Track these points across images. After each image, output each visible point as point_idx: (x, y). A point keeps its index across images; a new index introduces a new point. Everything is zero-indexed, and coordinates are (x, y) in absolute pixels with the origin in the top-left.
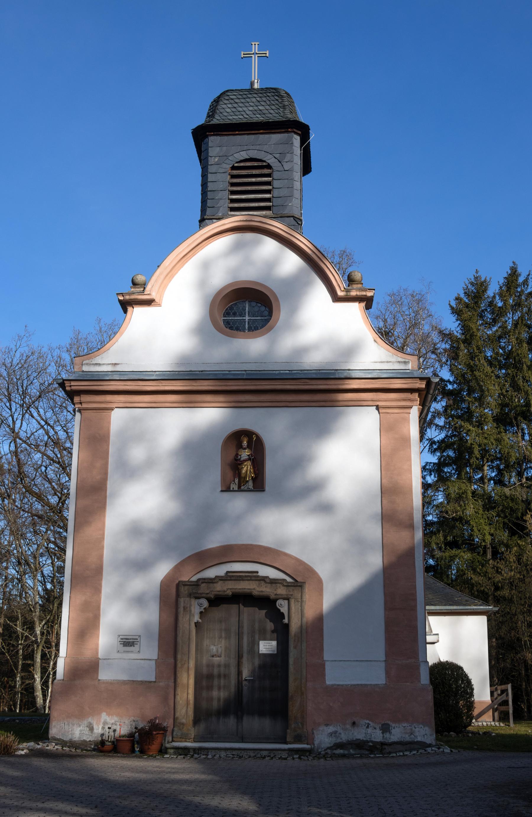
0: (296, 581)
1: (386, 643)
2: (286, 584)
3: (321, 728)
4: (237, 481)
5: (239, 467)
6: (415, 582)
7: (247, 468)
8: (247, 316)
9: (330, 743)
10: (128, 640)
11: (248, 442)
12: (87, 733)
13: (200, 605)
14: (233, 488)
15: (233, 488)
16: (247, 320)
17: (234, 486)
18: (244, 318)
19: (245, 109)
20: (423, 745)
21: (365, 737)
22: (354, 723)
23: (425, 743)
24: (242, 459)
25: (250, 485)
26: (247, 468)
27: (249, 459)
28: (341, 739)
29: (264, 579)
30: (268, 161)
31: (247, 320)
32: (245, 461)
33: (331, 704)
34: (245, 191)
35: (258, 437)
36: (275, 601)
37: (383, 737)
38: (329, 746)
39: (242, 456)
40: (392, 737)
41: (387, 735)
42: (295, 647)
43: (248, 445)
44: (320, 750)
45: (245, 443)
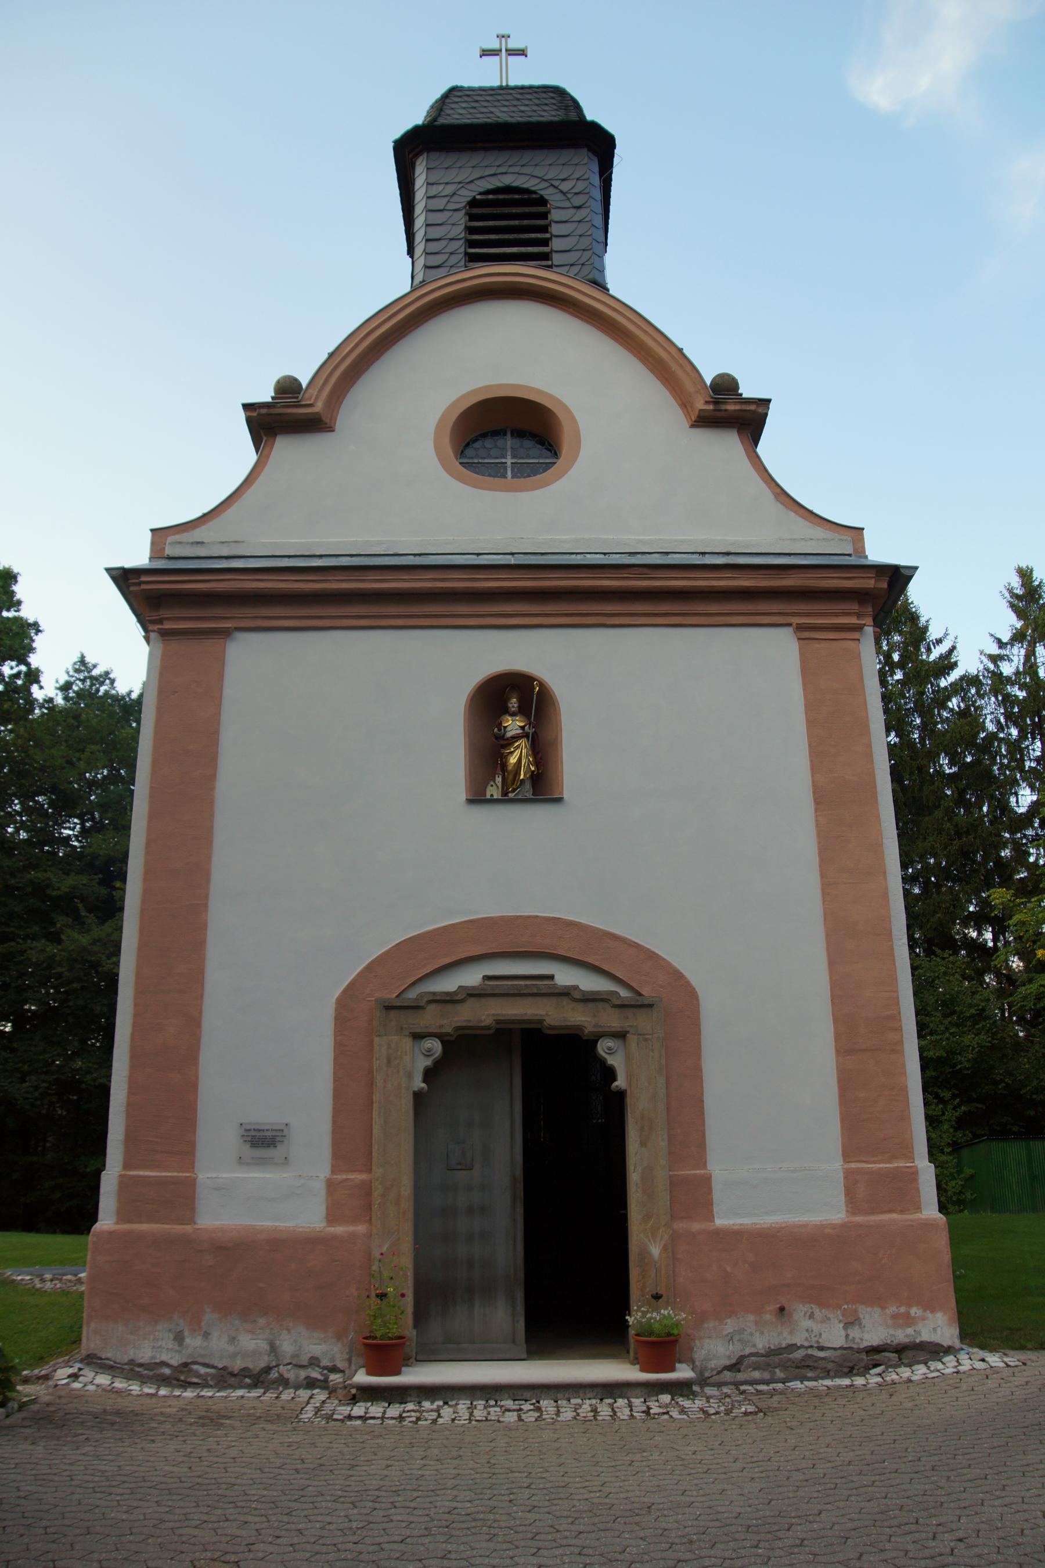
0: (640, 994)
1: (842, 1127)
2: (618, 1002)
3: (710, 1324)
4: (499, 780)
5: (503, 751)
6: (897, 991)
7: (518, 755)
8: (509, 457)
9: (729, 1357)
10: (262, 1134)
11: (520, 701)
12: (170, 1346)
13: (428, 1053)
14: (492, 795)
15: (492, 795)
16: (509, 464)
17: (494, 791)
18: (504, 461)
19: (492, 109)
20: (935, 1351)
21: (806, 1339)
22: (782, 1309)
23: (938, 1345)
24: (509, 734)
25: (527, 791)
26: (518, 755)
27: (526, 735)
28: (754, 1346)
29: (566, 993)
30: (542, 193)
31: (509, 464)
32: (516, 738)
33: (729, 1269)
34: (495, 206)
35: (542, 685)
36: (593, 1043)
37: (847, 1336)
38: (728, 1363)
39: (509, 729)
40: (866, 1336)
41: (855, 1333)
42: (643, 1144)
43: (519, 707)
44: (707, 1374)
45: (514, 703)
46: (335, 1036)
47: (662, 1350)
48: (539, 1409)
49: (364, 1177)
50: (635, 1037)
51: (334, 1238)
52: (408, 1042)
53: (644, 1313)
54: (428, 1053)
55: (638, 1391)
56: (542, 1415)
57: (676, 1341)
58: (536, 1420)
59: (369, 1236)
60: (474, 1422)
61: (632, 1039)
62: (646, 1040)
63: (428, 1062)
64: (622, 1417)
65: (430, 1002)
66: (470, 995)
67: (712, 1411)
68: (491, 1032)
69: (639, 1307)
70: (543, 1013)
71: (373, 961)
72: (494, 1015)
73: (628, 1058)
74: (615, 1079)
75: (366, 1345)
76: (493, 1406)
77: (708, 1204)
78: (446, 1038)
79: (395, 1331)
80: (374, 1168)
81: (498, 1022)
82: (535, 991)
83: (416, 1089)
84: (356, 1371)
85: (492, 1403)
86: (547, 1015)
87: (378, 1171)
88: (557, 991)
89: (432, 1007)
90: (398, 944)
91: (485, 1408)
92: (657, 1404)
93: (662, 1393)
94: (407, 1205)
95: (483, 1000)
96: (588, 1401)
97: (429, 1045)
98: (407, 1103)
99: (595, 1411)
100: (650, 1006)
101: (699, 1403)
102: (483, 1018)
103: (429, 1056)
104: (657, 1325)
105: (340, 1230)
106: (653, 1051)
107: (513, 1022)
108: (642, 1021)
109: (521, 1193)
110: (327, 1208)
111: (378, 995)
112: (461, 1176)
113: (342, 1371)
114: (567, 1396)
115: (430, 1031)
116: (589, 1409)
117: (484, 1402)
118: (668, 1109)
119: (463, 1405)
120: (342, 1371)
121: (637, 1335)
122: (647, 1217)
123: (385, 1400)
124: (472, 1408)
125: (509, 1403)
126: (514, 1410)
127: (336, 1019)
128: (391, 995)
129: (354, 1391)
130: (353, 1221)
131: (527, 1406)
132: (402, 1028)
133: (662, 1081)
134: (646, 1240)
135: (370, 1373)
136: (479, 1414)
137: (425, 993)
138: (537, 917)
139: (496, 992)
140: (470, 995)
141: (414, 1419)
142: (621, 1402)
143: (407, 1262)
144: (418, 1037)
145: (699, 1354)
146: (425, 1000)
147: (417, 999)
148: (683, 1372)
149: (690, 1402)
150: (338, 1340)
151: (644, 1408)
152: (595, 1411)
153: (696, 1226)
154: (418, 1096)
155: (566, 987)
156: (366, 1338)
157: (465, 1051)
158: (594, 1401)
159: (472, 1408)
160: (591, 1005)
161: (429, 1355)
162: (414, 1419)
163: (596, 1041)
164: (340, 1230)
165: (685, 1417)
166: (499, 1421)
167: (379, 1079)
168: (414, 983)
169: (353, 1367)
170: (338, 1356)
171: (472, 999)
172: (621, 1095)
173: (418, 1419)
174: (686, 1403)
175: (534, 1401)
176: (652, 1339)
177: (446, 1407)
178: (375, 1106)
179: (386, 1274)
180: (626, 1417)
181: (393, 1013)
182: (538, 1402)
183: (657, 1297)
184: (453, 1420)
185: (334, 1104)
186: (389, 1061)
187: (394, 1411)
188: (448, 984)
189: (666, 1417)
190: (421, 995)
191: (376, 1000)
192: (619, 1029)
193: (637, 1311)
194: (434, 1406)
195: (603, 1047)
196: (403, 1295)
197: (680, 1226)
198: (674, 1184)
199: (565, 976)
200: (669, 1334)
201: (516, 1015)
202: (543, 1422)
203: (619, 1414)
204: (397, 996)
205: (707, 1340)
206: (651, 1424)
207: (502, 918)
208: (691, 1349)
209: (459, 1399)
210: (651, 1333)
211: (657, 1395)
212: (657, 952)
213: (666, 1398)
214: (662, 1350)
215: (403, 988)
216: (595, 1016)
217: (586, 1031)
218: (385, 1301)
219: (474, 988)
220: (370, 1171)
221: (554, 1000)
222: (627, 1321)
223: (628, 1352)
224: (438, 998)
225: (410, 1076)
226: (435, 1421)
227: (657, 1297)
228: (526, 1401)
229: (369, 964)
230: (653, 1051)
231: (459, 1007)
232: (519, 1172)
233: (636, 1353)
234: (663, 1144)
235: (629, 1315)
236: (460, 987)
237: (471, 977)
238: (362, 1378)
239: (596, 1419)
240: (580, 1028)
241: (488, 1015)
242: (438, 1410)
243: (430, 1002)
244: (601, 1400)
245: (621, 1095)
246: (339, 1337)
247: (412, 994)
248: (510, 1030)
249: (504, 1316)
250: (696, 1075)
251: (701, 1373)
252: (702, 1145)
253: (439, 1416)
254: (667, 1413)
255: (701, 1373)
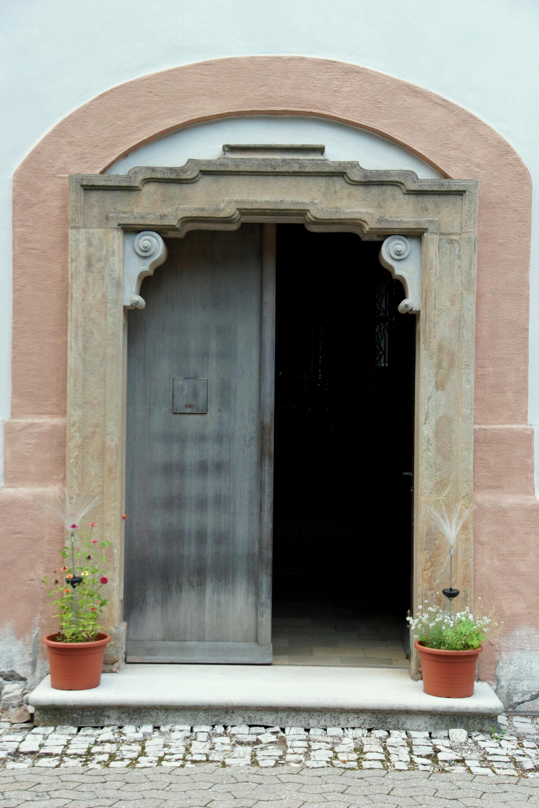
0: (445, 176)
13: (144, 254)
42: (440, 386)
44: (516, 699)
46: (14, 226)
47: (454, 667)
48: (282, 742)
49: (56, 421)
50: (436, 237)
51: (14, 502)
52: (117, 236)
53: (432, 616)
54: (144, 254)
55: (420, 721)
56: (285, 753)
57: (474, 657)
58: (277, 764)
59: (61, 501)
60: (188, 765)
61: (431, 240)
62: (451, 242)
63: (146, 267)
64: (398, 765)
65: (147, 181)
66: (205, 173)
67: (528, 765)
68: (234, 227)
69: (426, 606)
70: (307, 200)
71: (66, 120)
72: (237, 202)
73: (424, 268)
74: (403, 295)
75: (51, 648)
76: (221, 735)
77: (527, 470)
78: (171, 234)
79: (92, 627)
80: (69, 409)
81: (243, 212)
82: (296, 168)
83: (128, 304)
84: (42, 678)
85: (220, 729)
86: (312, 203)
87: (75, 414)
88: (327, 169)
89: (150, 188)
90: (102, 96)
91: (210, 737)
92: (447, 743)
93: (455, 727)
94: (117, 461)
95: (223, 180)
96: (350, 732)
97: (147, 243)
98: (117, 322)
99: (359, 750)
100: (460, 193)
101: (509, 746)
102: (222, 206)
103: (145, 258)
104: (450, 633)
105: (23, 492)
106: (459, 257)
107: (263, 212)
108: (444, 215)
109: (270, 446)
110: (5, 462)
111: (74, 170)
112: (191, 423)
113: (23, 679)
114: (322, 723)
115: (148, 222)
116: (352, 745)
117: (208, 728)
118: (477, 339)
119: (179, 731)
120: (23, 679)
121: (421, 643)
122: (440, 485)
123: (73, 724)
124: (191, 738)
125: (242, 731)
126: (248, 743)
127: (15, 202)
128: (92, 171)
129: (31, 709)
130: (43, 479)
131: (267, 737)
132: (107, 218)
133: (470, 300)
134: (438, 515)
135: (57, 685)
136: (199, 749)
137: (141, 168)
138: (303, 59)
139: (241, 169)
140: (205, 173)
141: (106, 757)
142: (397, 737)
143: (115, 538)
144: (130, 230)
145: (506, 672)
146: (140, 177)
147: (128, 177)
148: (483, 698)
149: (493, 743)
150: (18, 637)
151: (429, 751)
152: (359, 750)
153: (508, 500)
154: (132, 314)
155: (340, 163)
156: (52, 638)
157: (194, 253)
158: (359, 733)
159: (191, 738)
160: (375, 191)
161: (141, 654)
162: (106, 757)
163: (380, 243)
164: (23, 492)
165: (488, 771)
166: (224, 765)
167: (76, 291)
168: (126, 155)
169: (38, 674)
170: (17, 658)
171: (208, 178)
172: (412, 319)
173: (112, 757)
174: (488, 744)
175: (277, 729)
176: (443, 651)
177: (156, 734)
178: (71, 325)
179: (85, 551)
180: (404, 766)
181: (94, 196)
182: (283, 730)
183: (451, 594)
184: (161, 759)
185: (15, 322)
186: (89, 264)
187: (81, 742)
188: (172, 157)
189: (459, 769)
190: (135, 172)
191: (71, 177)
192: (413, 226)
193: (422, 611)
194: (139, 736)
195: (389, 251)
196: (104, 581)
197: (485, 498)
198: (481, 441)
199: (340, 149)
200: (467, 646)
201: (268, 202)
202: (285, 769)
203: (393, 758)
204: (102, 172)
205: (519, 653)
206: (440, 781)
207: (252, 60)
208: (496, 663)
209: (175, 723)
210: (440, 643)
211: (447, 728)
212: (475, 114)
213: (459, 734)
214: (454, 667)
215: (109, 161)
216: (380, 207)
217: (367, 228)
218: (79, 588)
219: (209, 162)
220: (64, 413)
221: (322, 182)
222: (408, 622)
223: (408, 657)
224: (159, 176)
225: (118, 285)
226: (135, 761)
227: (451, 594)
228: (266, 727)
229: (61, 124)
230: (459, 257)
231: (187, 188)
232: (269, 419)
233: (419, 665)
234: (469, 387)
235: (412, 615)
236: (189, 161)
237: (206, 147)
238: (46, 693)
239: (360, 767)
240: (358, 223)
241: (229, 202)
242: (142, 743)
243: (147, 181)
244: (370, 730)
245: (412, 319)
246: (19, 634)
247: (122, 170)
248: (262, 225)
249: (245, 605)
250: (520, 293)
251: (509, 696)
252: (522, 391)
253: (143, 753)
254: (462, 761)
255: (509, 696)
